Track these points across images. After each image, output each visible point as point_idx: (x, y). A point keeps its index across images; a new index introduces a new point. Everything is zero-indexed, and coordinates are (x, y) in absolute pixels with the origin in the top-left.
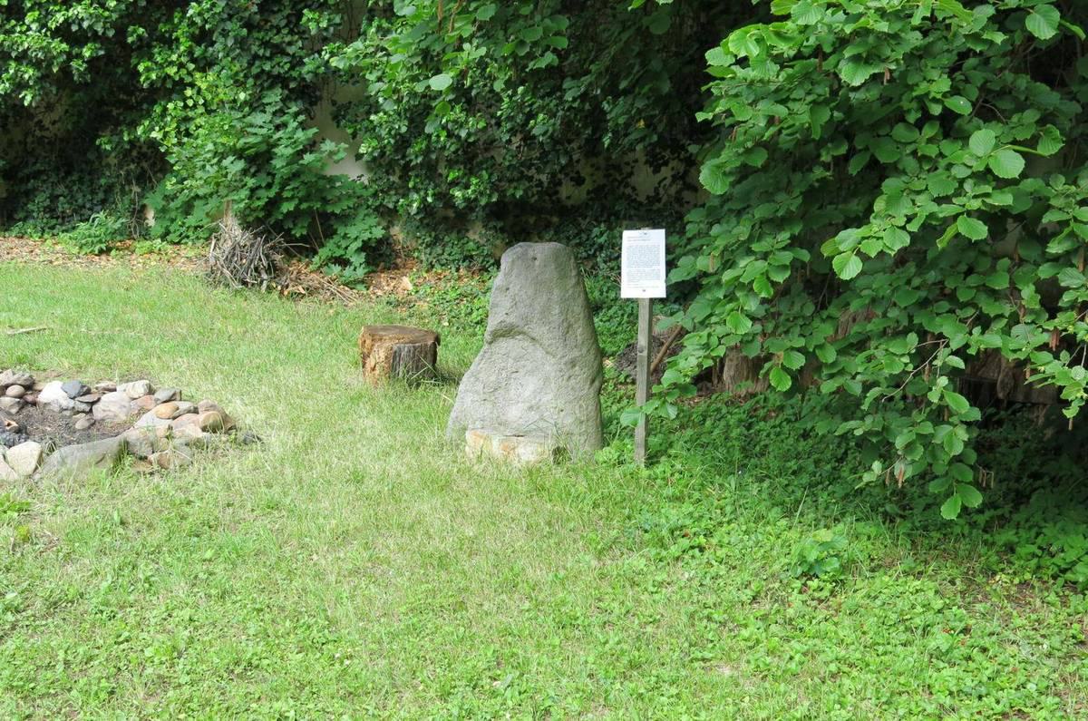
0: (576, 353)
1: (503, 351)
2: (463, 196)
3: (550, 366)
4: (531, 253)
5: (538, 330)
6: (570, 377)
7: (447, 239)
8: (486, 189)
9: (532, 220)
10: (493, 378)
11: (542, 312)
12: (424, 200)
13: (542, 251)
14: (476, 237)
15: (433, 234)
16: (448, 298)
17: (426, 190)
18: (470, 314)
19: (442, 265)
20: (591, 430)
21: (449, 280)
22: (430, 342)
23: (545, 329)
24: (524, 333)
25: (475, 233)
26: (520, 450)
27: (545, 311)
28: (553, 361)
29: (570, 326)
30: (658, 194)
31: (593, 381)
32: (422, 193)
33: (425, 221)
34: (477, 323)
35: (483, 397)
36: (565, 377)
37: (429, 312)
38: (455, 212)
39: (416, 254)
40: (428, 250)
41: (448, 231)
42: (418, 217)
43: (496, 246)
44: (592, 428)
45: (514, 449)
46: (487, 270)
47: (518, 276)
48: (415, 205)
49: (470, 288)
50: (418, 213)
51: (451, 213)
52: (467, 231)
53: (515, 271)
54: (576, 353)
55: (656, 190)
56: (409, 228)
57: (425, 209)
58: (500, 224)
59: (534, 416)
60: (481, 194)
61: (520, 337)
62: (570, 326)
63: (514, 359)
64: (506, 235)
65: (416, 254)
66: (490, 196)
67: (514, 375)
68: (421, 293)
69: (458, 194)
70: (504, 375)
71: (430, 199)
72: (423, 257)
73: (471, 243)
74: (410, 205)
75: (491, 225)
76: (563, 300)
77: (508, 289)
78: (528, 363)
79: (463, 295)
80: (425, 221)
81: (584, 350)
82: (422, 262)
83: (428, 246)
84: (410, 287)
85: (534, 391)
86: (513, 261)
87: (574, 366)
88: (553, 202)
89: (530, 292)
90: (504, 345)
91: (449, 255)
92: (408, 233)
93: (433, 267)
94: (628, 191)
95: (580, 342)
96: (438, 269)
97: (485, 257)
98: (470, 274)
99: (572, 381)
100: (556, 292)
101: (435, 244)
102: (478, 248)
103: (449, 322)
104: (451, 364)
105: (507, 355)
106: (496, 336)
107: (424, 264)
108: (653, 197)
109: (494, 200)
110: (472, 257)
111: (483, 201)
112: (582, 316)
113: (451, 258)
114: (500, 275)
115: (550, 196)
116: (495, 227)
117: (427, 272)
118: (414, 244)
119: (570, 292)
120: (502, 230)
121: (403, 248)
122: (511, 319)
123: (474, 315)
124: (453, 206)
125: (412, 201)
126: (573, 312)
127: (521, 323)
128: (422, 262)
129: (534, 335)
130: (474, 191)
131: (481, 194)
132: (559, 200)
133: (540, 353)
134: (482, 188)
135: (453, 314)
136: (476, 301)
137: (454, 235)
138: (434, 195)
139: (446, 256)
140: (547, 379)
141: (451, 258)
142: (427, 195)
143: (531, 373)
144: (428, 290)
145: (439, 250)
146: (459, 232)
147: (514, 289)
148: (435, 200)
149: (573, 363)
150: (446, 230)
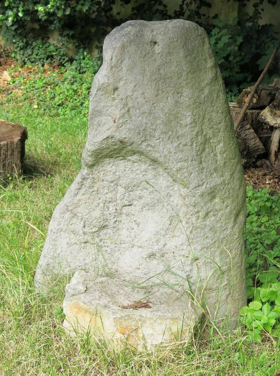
0: (216, 180)
1: (109, 177)
2: (45, 10)
3: (178, 197)
4: (148, 35)
5: (162, 148)
6: (207, 214)
7: (34, 44)
8: (61, 5)
9: (93, 30)
10: (97, 213)
11: (167, 123)
12: (16, 15)
13: (164, 31)
14: (55, 42)
15: (25, 40)
16: (37, 86)
17: (18, 7)
18: (53, 98)
19: (32, 62)
20: (235, 281)
21: (37, 73)
22: (17, 139)
23: (171, 147)
24: (141, 153)
25: (54, 40)
26: (146, 330)
27: (172, 119)
28: (184, 191)
29: (206, 141)
30: (183, 9)
31: (237, 216)
32: (15, 10)
33: (19, 32)
34: (59, 105)
35: (82, 238)
36: (202, 214)
37: (23, 98)
38: (39, 25)
39: (13, 55)
40: (22, 52)
41: (35, 38)
42: (13, 28)
43: (68, 49)
44: (235, 277)
45: (136, 330)
46: (63, 65)
47: (131, 69)
48: (10, 19)
49: (52, 78)
50: (12, 25)
51: (37, 26)
52: (49, 38)
53: (126, 62)
54: (216, 180)
55: (181, 7)
56: (8, 37)
57: (17, 21)
58: (71, 33)
59: (156, 266)
60: (58, 8)
61: (135, 157)
62: (206, 141)
63: (126, 188)
64: (75, 41)
65: (13, 55)
66: (64, 10)
67: (125, 210)
68: (17, 82)
69: (41, 8)
70: (112, 209)
71: (20, 14)
72: (18, 57)
73: (52, 47)
74: (7, 19)
75: (65, 33)
76: (198, 104)
77: (116, 89)
78: (145, 193)
79: (47, 84)
80: (19, 32)
81: (227, 175)
82: (17, 60)
83: (21, 49)
84: (9, 79)
85: (157, 233)
86: (123, 47)
87: (214, 197)
88: (107, 17)
89: (150, 92)
90: (112, 169)
91: (37, 55)
92: (7, 40)
93: (25, 63)
94: (161, 8)
95: (220, 162)
96: (29, 65)
97: (62, 56)
98: (52, 68)
99: (211, 219)
100: (187, 92)
101: (26, 47)
102: (57, 50)
103: (38, 104)
104: (39, 151)
105: (115, 182)
106: (101, 156)
107: (19, 62)
108: (179, 11)
109: (68, 13)
110: (52, 56)
111: (60, 14)
112: (222, 126)
113: (38, 57)
114: (104, 71)
115: (106, 12)
116: (68, 35)
117: (22, 67)
118: (12, 48)
119: (206, 91)
120: (73, 37)
121: (4, 50)
122: (123, 134)
123: (57, 99)
124: (39, 20)
125: (8, 17)
126: (210, 120)
127: (137, 139)
128: (17, 60)
129: (156, 155)
130: (53, 6)
131: (58, 8)
132: (111, 16)
133: (163, 181)
134: (58, 4)
135: (41, 99)
136: (57, 88)
137: (39, 41)
138: (23, 11)
139: (34, 56)
140: (174, 219)
141: (38, 57)
142: (18, 11)
143: (151, 206)
144: (22, 81)
145: (29, 51)
146: (42, 39)
147: (125, 89)
148: (24, 15)
149: (212, 194)
150: (34, 38)
